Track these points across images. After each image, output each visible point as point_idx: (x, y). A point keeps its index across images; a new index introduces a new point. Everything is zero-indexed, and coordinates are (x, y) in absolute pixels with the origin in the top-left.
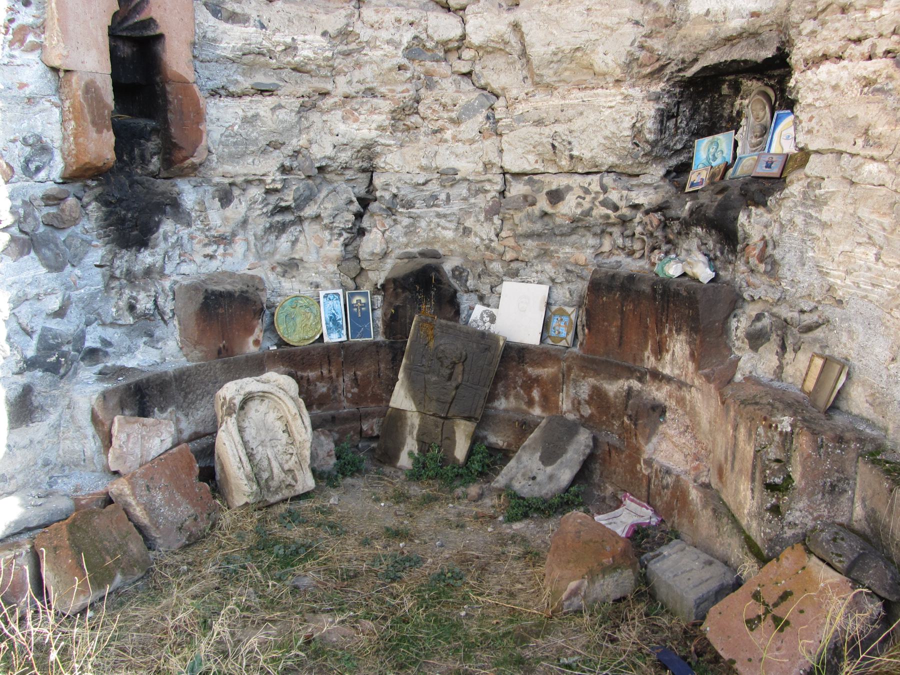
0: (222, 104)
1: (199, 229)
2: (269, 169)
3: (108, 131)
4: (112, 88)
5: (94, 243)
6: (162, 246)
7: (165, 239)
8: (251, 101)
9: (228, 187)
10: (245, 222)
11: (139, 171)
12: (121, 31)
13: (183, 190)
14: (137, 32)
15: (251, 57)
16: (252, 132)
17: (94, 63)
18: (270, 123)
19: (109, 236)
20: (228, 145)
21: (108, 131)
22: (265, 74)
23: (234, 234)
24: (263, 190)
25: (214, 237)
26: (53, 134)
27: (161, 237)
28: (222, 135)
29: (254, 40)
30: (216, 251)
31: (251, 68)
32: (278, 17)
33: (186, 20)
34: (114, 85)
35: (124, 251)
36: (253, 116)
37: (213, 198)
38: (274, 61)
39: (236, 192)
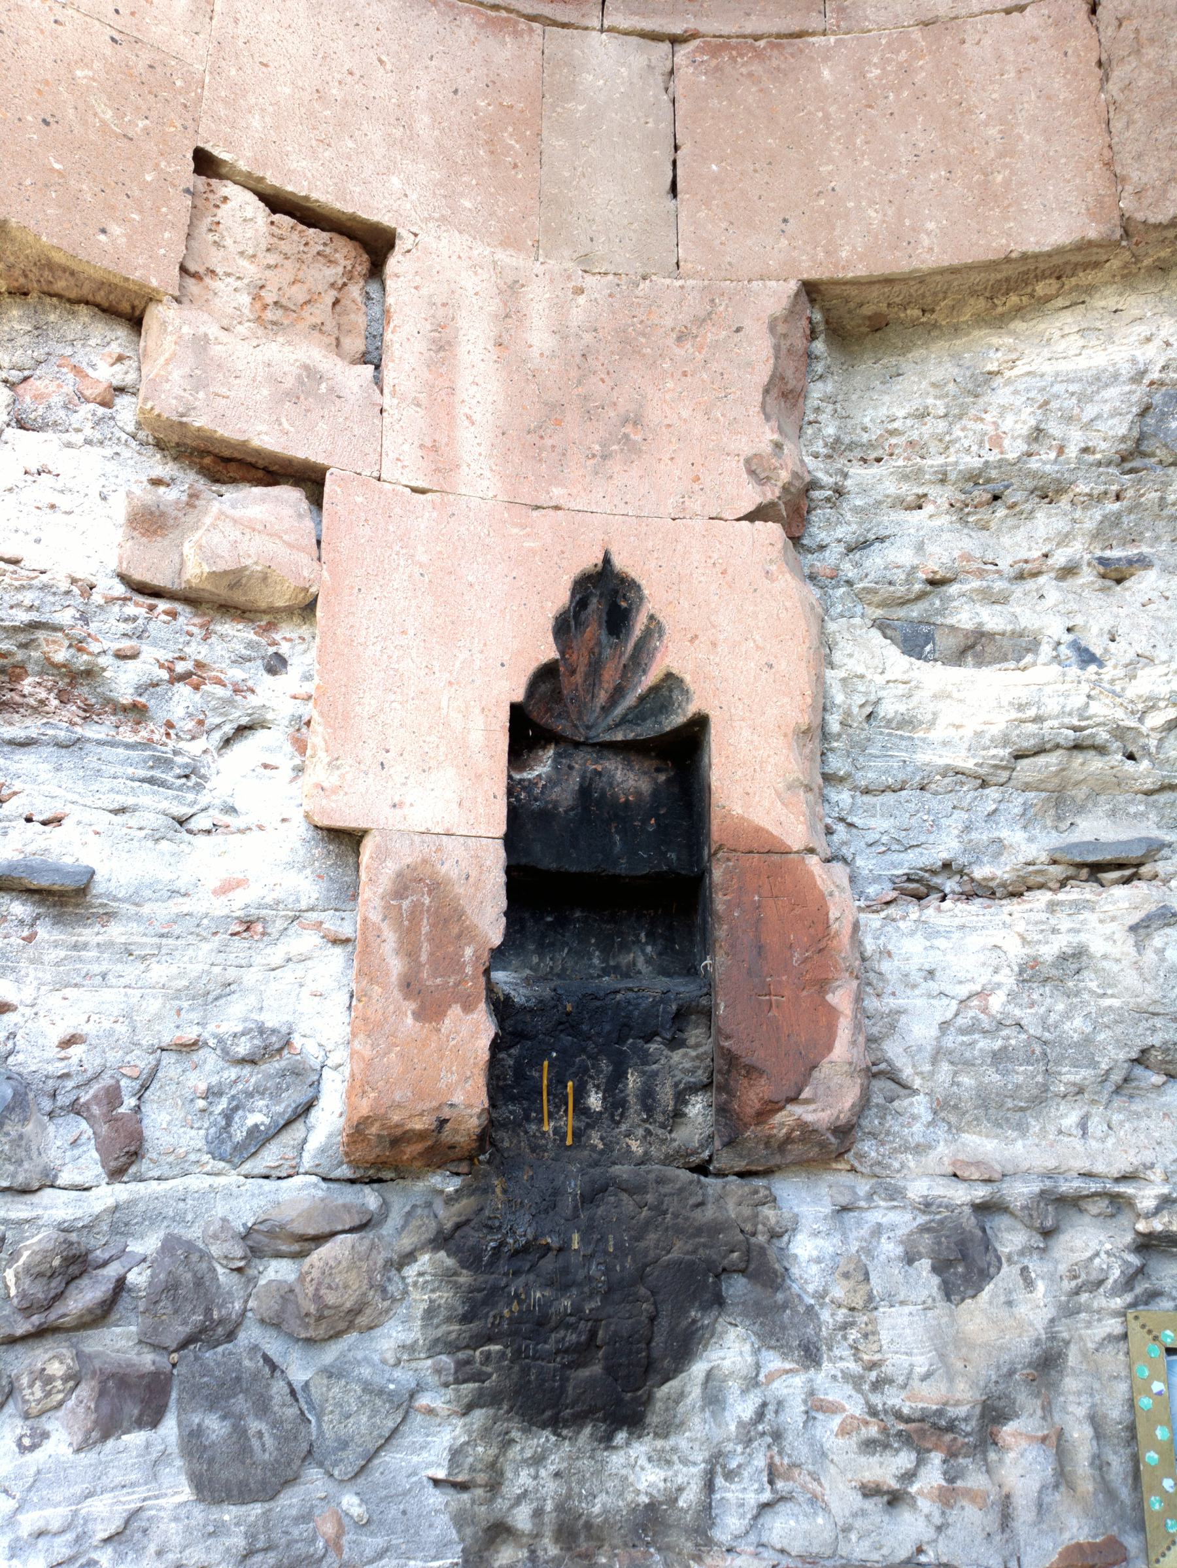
1: (847, 1376)
2: (1148, 1156)
3: (468, 1008)
4: (502, 879)
6: (695, 1436)
7: (714, 1399)
8: (1052, 907)
9: (969, 1221)
10: (1047, 1364)
11: (636, 1147)
14: (649, 723)
15: (1052, 760)
16: (1067, 1015)
17: (451, 807)
18: (1131, 979)
19: (479, 1377)
20: (969, 1064)
21: (468, 1008)
22: (1113, 813)
23: (994, 1413)
24: (1129, 1238)
25: (899, 1416)
28: (944, 1026)
29: (1052, 706)
30: (909, 1476)
31: (1060, 801)
32: (1144, 619)
33: (782, 666)
34: (509, 870)
35: (545, 1437)
36: (1063, 958)
37: (910, 1259)
38: (1145, 764)
39: (1011, 1239)
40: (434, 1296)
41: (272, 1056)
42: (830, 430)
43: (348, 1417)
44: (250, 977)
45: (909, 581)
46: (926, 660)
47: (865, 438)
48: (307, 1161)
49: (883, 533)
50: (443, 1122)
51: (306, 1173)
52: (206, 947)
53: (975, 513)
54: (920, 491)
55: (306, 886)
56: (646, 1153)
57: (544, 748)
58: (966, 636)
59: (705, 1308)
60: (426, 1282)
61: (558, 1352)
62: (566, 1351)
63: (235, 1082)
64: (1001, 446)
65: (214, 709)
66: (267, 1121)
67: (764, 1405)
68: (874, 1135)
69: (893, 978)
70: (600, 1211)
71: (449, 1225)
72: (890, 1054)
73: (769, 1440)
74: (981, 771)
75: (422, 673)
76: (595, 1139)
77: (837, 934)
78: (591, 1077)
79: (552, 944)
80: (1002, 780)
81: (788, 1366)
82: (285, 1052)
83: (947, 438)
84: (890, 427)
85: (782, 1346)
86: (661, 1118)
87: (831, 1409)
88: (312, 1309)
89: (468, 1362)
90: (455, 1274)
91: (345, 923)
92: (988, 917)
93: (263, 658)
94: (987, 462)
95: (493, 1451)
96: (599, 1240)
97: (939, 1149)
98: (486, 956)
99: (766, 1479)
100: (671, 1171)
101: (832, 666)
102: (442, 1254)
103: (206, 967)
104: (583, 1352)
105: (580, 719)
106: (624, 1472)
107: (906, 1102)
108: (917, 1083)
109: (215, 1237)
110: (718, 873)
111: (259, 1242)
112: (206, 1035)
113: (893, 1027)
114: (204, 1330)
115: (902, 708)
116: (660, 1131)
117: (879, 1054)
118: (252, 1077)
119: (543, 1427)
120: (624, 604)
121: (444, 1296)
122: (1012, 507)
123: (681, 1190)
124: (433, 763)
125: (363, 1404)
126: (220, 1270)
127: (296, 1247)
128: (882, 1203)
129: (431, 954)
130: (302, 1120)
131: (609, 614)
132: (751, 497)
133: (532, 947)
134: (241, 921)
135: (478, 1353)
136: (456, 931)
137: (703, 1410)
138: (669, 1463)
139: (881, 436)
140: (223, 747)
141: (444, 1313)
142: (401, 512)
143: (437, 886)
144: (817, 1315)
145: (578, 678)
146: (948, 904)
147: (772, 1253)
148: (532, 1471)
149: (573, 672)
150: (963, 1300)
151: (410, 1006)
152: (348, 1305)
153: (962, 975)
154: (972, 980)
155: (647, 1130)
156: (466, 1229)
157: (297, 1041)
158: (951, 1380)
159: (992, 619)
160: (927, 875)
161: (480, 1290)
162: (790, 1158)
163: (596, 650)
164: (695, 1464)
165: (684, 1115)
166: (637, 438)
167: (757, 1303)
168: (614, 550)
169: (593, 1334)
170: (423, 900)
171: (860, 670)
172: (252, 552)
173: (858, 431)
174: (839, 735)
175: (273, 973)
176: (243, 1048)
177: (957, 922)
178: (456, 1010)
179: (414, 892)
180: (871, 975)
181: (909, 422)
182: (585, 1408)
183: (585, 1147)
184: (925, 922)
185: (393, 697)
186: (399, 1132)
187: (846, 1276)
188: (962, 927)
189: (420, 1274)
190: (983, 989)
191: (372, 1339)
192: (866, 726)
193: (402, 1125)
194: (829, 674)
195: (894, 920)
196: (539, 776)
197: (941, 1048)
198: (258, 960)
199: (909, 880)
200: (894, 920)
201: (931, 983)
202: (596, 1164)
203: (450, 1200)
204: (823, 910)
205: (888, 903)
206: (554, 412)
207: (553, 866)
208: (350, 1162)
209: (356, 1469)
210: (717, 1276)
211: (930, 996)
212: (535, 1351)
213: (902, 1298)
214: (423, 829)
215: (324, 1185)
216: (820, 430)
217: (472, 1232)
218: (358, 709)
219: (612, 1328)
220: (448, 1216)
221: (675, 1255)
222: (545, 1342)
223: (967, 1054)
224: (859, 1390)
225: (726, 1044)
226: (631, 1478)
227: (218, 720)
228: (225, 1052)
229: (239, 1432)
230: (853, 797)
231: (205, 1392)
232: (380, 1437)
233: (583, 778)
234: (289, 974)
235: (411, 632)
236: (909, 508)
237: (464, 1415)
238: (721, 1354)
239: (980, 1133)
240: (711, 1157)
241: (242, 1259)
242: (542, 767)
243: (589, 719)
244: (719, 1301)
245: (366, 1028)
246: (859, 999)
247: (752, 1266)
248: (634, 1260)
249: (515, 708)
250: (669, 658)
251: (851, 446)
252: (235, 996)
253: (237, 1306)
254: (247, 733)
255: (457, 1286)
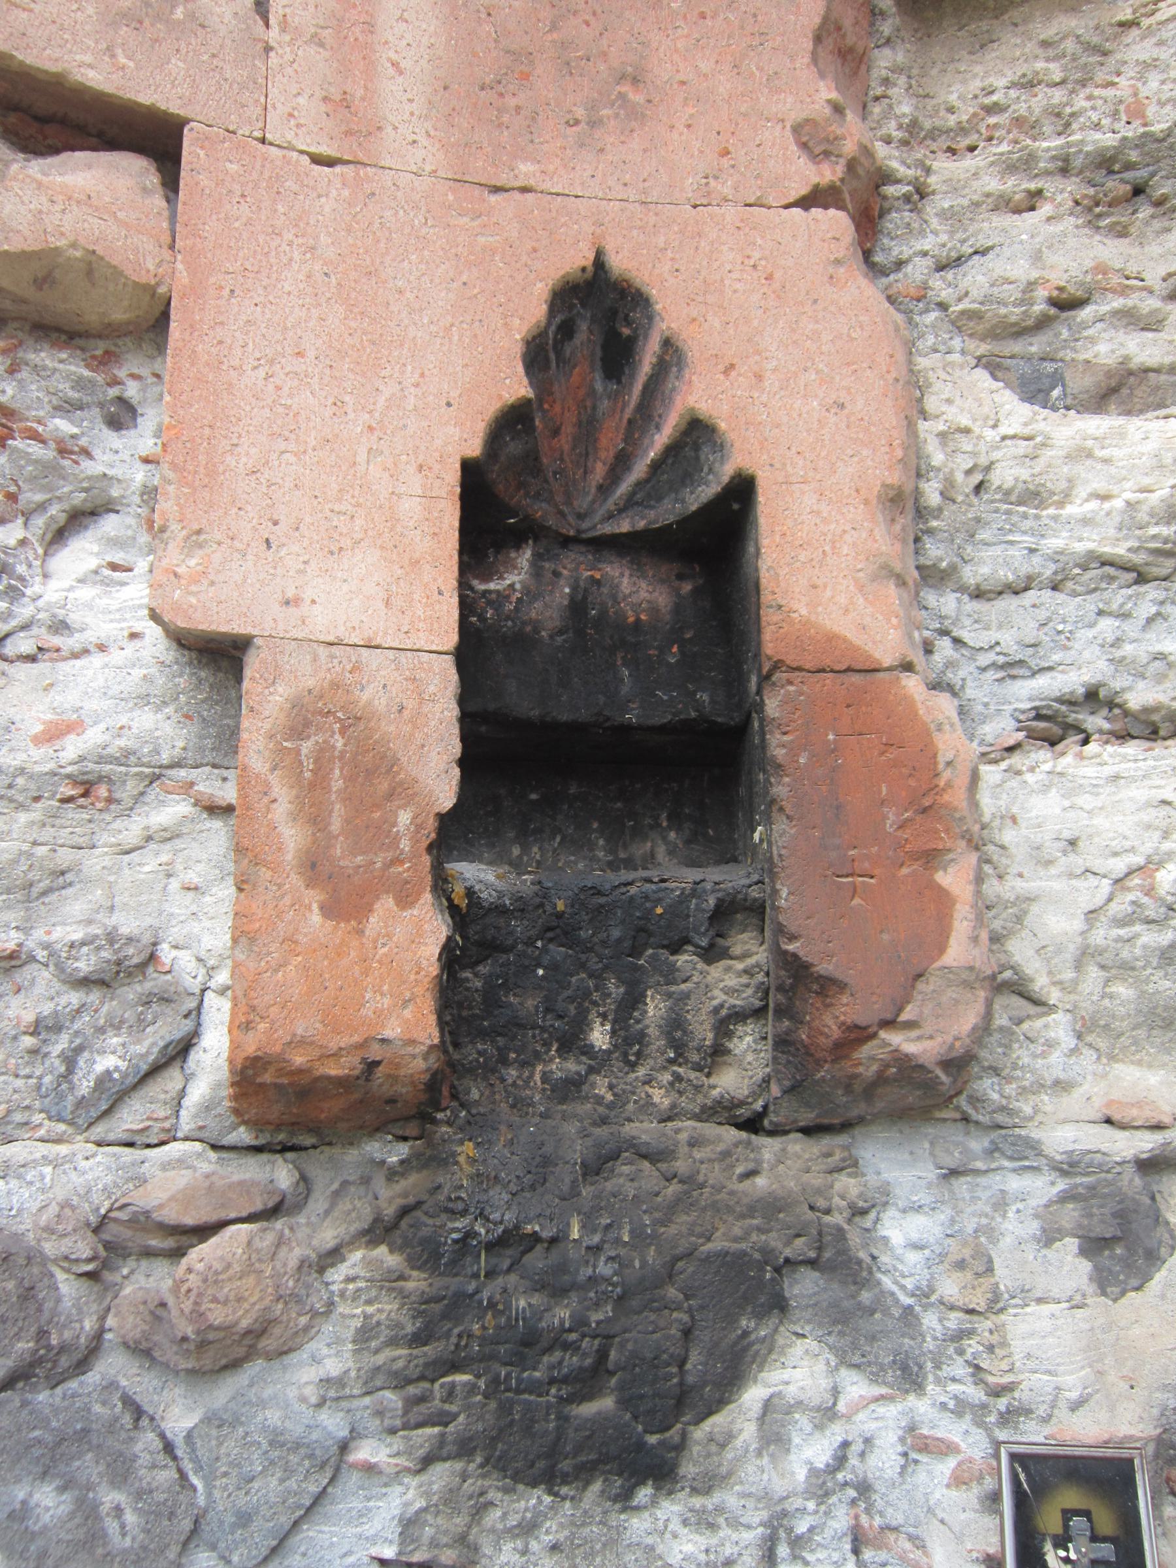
0: (1089, 771)
5: (364, 1452)
12: (610, 516)
13: (885, 1191)
14: (667, 503)
17: (371, 606)
19: (443, 1419)
20: (1127, 967)
21: (405, 900)
26: (198, 932)
27: (748, 1432)
28: (1092, 915)
35: (535, 1499)
37: (1049, 1238)
40: (370, 1309)
41: (130, 975)
42: (905, 109)
43: (252, 1480)
44: (95, 862)
45: (1026, 300)
46: (1055, 409)
47: (952, 120)
48: (186, 1123)
49: (982, 242)
50: (372, 1066)
51: (186, 1139)
52: (23, 817)
53: (1108, 215)
54: (1032, 186)
55: (162, 730)
56: (673, 1106)
57: (518, 547)
58: (1109, 374)
59: (760, 1315)
60: (358, 1290)
61: (552, 1381)
62: (565, 1380)
63: (78, 1011)
64: (1144, 116)
65: (32, 479)
66: (123, 1065)
67: (845, 1444)
68: (996, 1071)
69: (1019, 852)
70: (609, 1186)
71: (389, 1211)
72: (1017, 958)
73: (852, 1493)
74: (1139, 559)
75: (328, 412)
76: (601, 1086)
77: (949, 785)
78: (595, 1004)
79: (539, 831)
80: (1164, 572)
81: (884, 1390)
82: (151, 969)
83: (1068, 110)
84: (987, 101)
85: (870, 1364)
86: (695, 1057)
87: (945, 1449)
88: (189, 1331)
89: (422, 1399)
90: (402, 1278)
91: (229, 784)
92: (1151, 763)
93: (101, 405)
94: (1125, 139)
95: (460, 1521)
96: (608, 1227)
97: (1086, 1087)
98: (431, 824)
99: (848, 1547)
100: (709, 1129)
101: (924, 415)
102: (382, 1251)
103: (25, 847)
104: (586, 1382)
105: (568, 503)
106: (649, 1540)
107: (1039, 1023)
108: (1054, 996)
109: (49, 1230)
110: (772, 706)
111: (121, 1239)
112: (30, 944)
113: (1019, 919)
114: (36, 1362)
115: (1024, 474)
116: (693, 1075)
117: (1003, 958)
118: (107, 1007)
119: (534, 1484)
120: (626, 331)
121: (386, 1308)
122: (1158, 203)
123: (726, 1154)
124: (346, 542)
125: (272, 1463)
126: (60, 1276)
127: (170, 1243)
128: (1006, 1163)
129: (347, 821)
130: (178, 1063)
131: (605, 347)
132: (807, 174)
133: (511, 835)
134: (73, 780)
135: (437, 1386)
136: (384, 786)
137: (759, 1454)
138: (712, 1527)
139: (975, 115)
140: (52, 543)
141: (385, 1334)
142: (295, 188)
143: (354, 721)
144: (917, 1317)
145: (564, 441)
146: (1092, 747)
147: (854, 1238)
148: (519, 1544)
149: (556, 432)
150: (1123, 1293)
151: (314, 898)
152: (244, 1324)
153: (1115, 845)
154: (1132, 850)
155: (674, 1073)
156: (418, 1213)
157: (166, 954)
158: (1112, 1409)
159: (1143, 349)
160: (1064, 708)
161: (438, 1299)
162: (880, 1105)
163: (588, 404)
164: (749, 1527)
165: (728, 1052)
166: (638, 98)
167: (835, 1305)
168: (610, 247)
169: (602, 1355)
170: (340, 747)
171: (965, 421)
172: (67, 228)
173: (942, 113)
174: (940, 509)
175: (127, 858)
176: (84, 965)
177: (1108, 771)
178: (387, 903)
179: (319, 729)
180: (990, 848)
181: (1013, 93)
182: (593, 1456)
183: (587, 1098)
184: (1061, 774)
185: (283, 446)
186: (305, 1080)
187: (961, 1265)
188: (1116, 778)
189: (350, 1279)
190: (1149, 861)
191: (285, 1368)
192: (975, 501)
193: (308, 1071)
194: (922, 426)
195: (1018, 773)
196: (512, 586)
197: (1088, 946)
198: (104, 838)
199: (1039, 717)
200: (1018, 773)
201: (1072, 857)
202: (604, 1121)
203: (393, 1175)
204: (929, 752)
205: (1010, 749)
206: (518, 65)
207: (535, 713)
208: (244, 1123)
209: (264, 1552)
210: (777, 1270)
211: (1071, 875)
212: (519, 1381)
213: (1039, 1295)
214: (331, 638)
215: (213, 1155)
216: (890, 107)
217: (425, 1219)
218: (230, 460)
219: (630, 1346)
220: (389, 1197)
221: (717, 1244)
222: (535, 1369)
223: (1125, 954)
224: (979, 1423)
225: (791, 947)
226: (660, 1549)
227: (39, 497)
228: (60, 968)
229: (87, 1510)
230: (959, 600)
231: (37, 1452)
232: (299, 1507)
233: (575, 588)
234: (150, 862)
235: (311, 354)
236: (1018, 211)
237: (419, 1472)
238: (786, 1374)
239: (1139, 1063)
240: (765, 1107)
241: (89, 1260)
242: (515, 575)
243: (582, 504)
244: (779, 1305)
245: (265, 928)
246: (979, 879)
247: (827, 1255)
248: (659, 1252)
249: (469, 469)
250: (698, 394)
251: (933, 134)
252: (69, 891)
253: (89, 1325)
254: (86, 521)
255: (403, 1295)
